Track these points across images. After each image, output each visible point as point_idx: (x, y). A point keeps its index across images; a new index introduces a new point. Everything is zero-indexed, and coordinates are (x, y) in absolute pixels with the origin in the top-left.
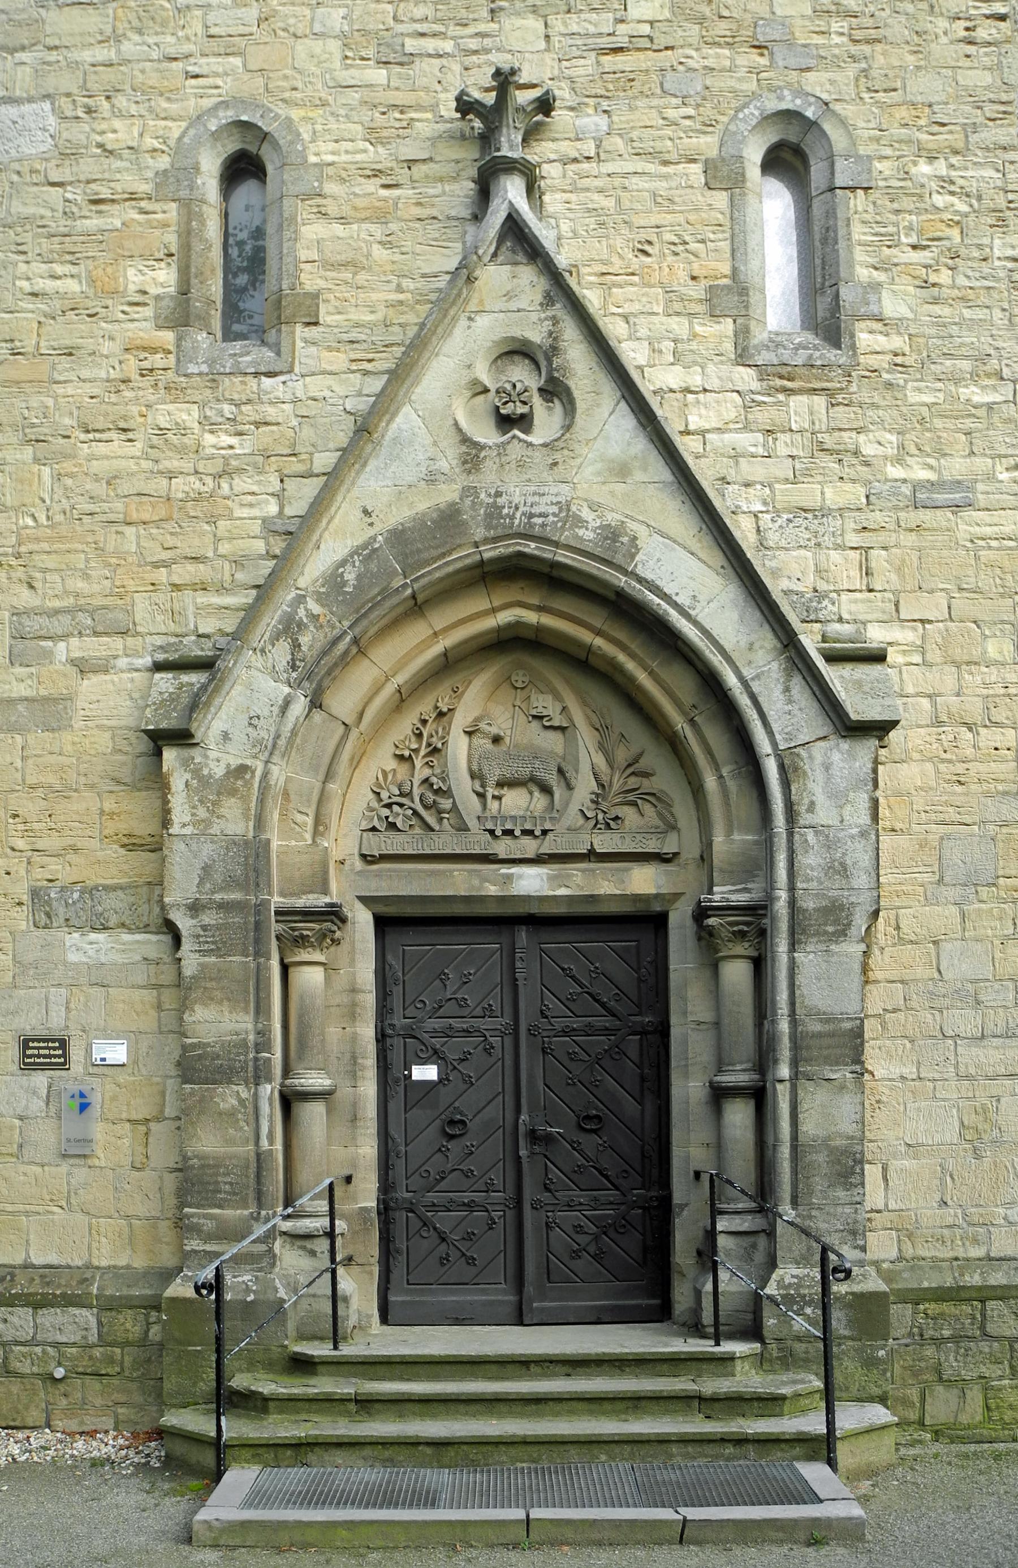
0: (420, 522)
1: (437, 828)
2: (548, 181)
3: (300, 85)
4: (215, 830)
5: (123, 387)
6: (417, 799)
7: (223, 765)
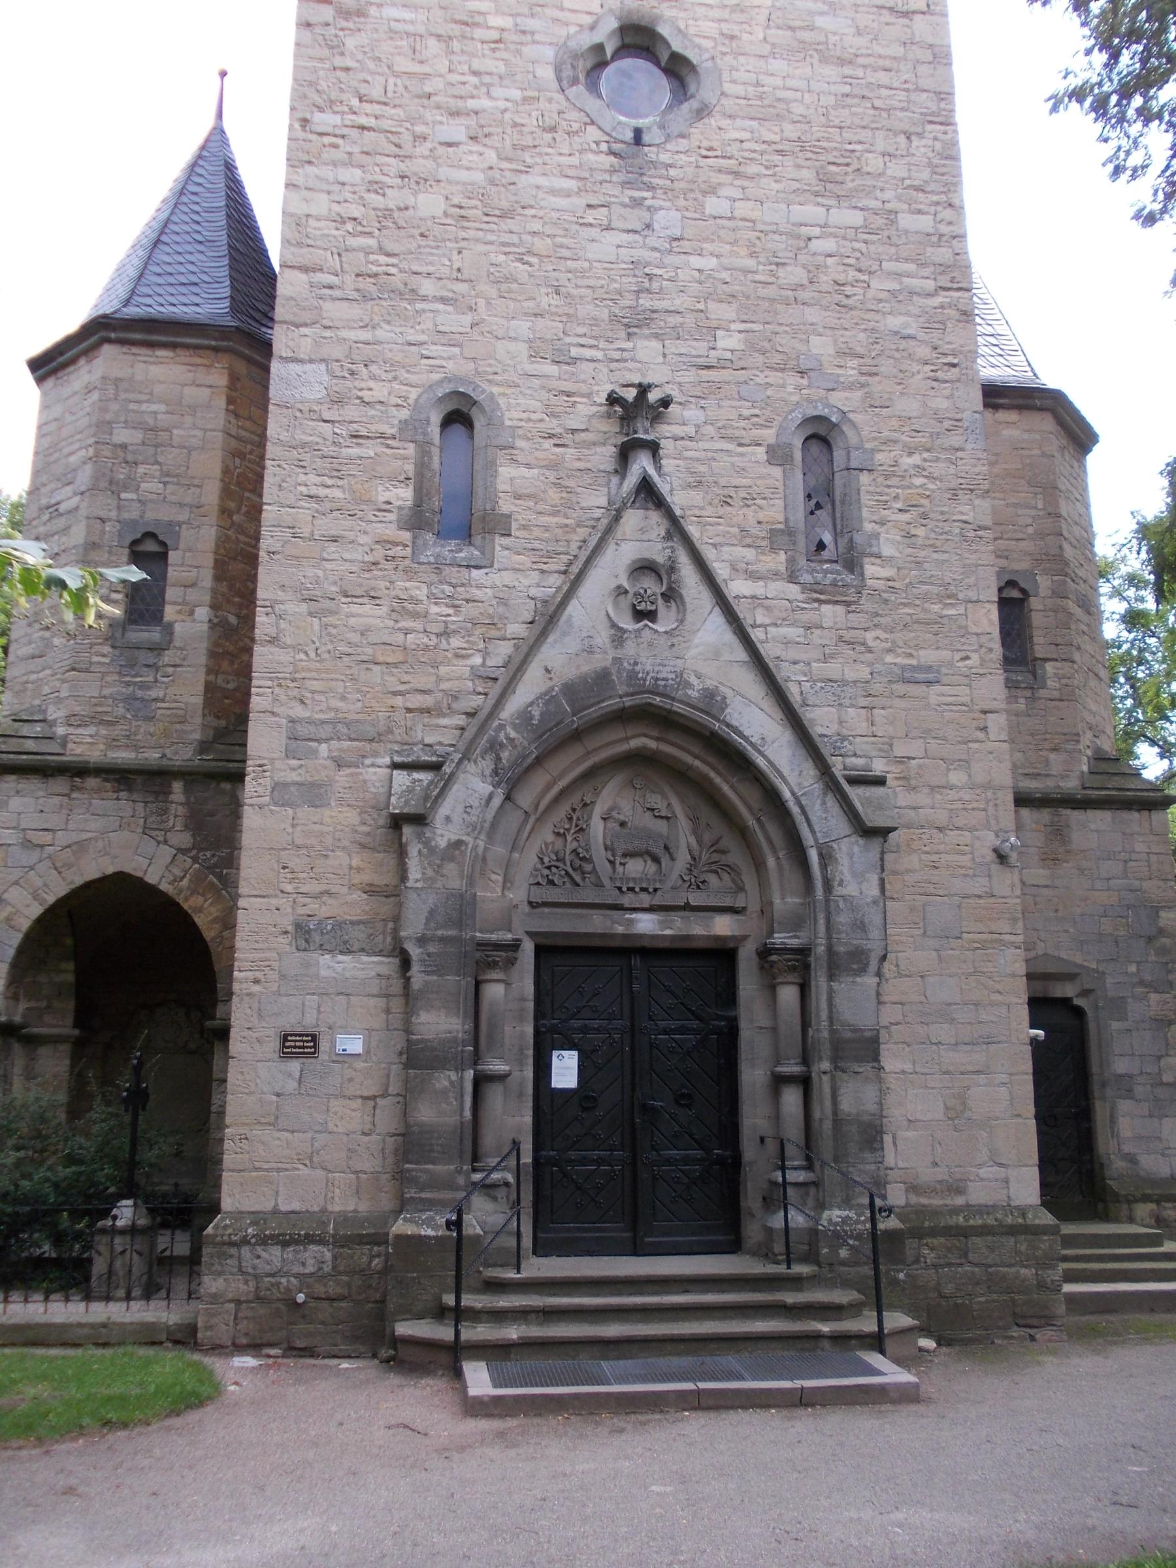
0: (583, 679)
1: (581, 884)
2: (665, 451)
3: (499, 371)
4: (439, 885)
5: (373, 567)
6: (568, 864)
7: (446, 839)
